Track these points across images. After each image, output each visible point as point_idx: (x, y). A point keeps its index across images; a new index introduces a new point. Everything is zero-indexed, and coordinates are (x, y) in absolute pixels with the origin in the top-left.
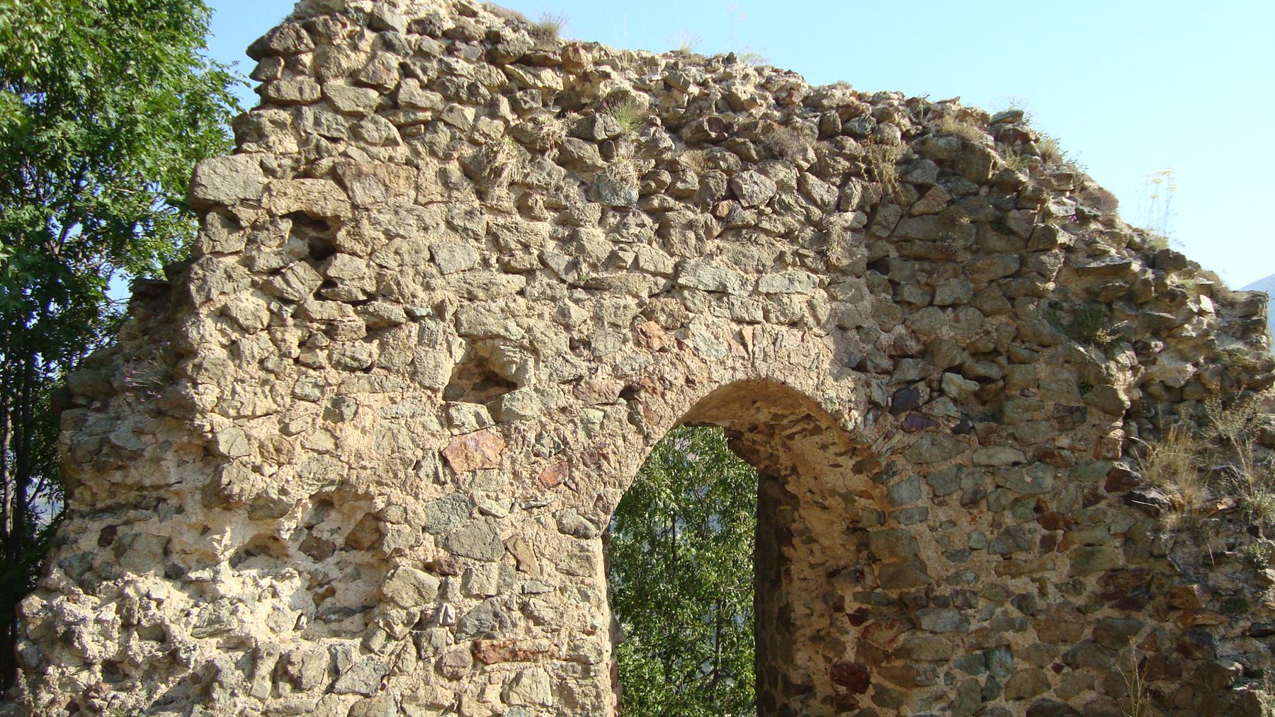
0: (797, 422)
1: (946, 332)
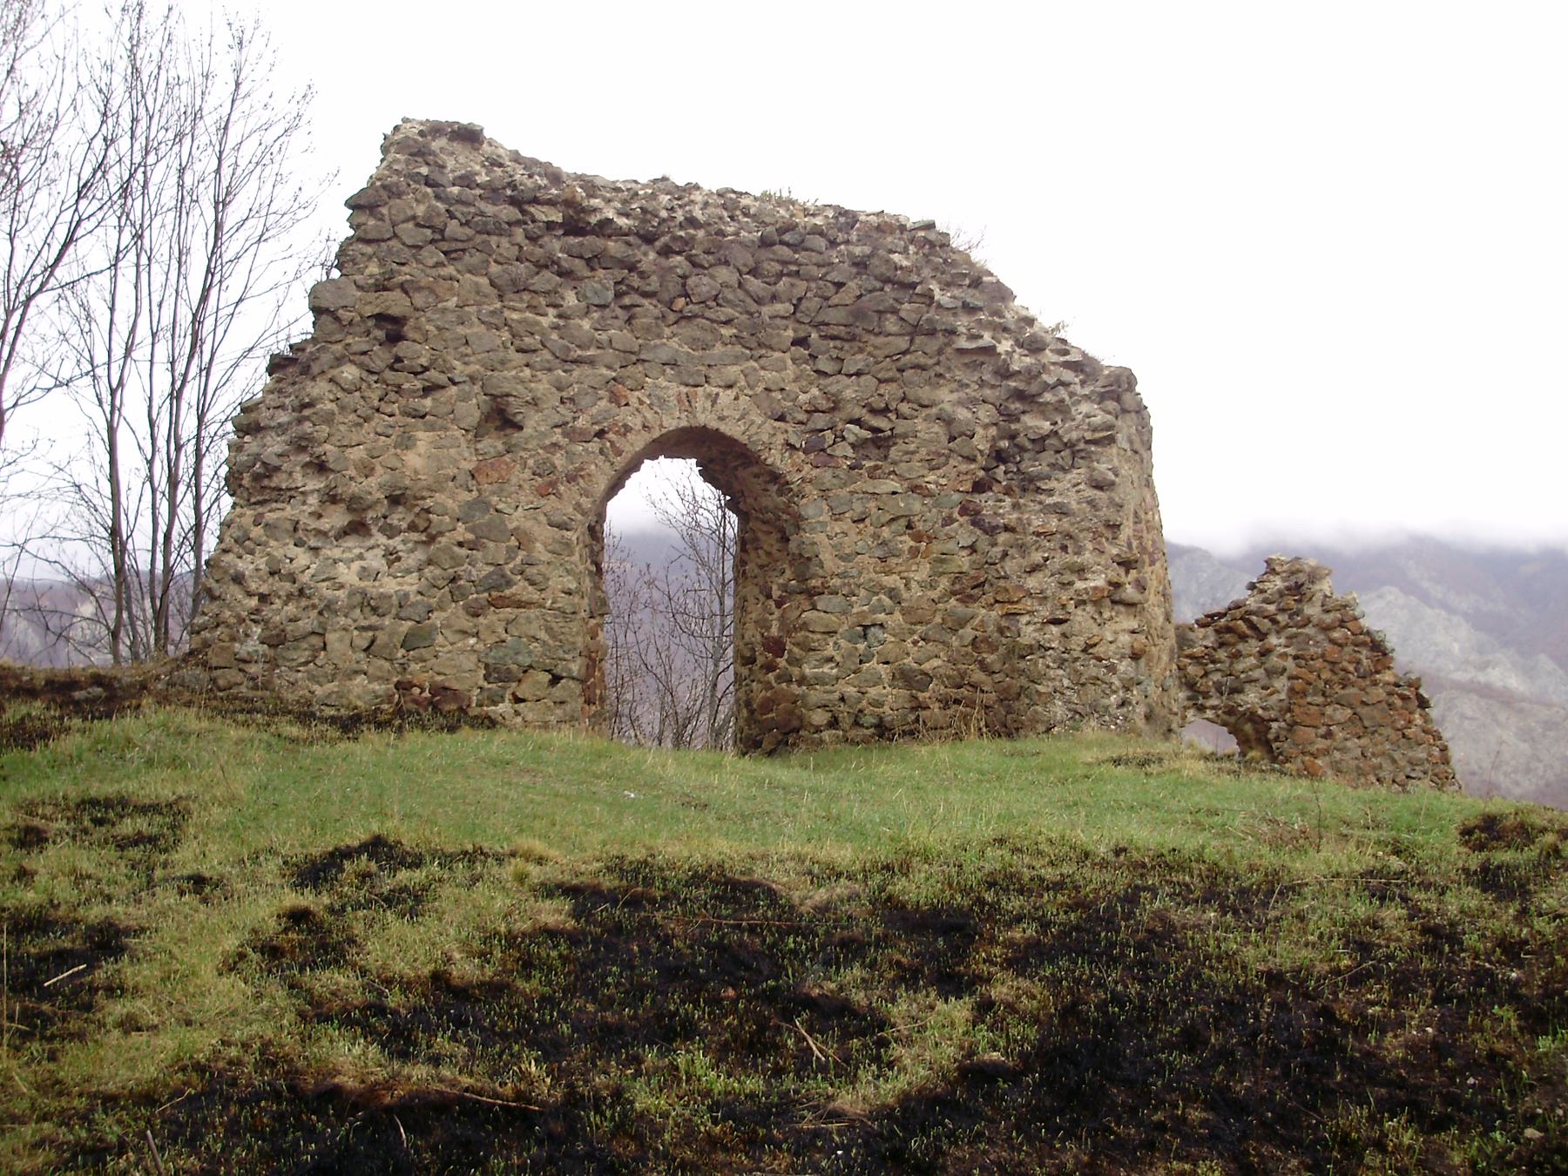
1: (849, 394)
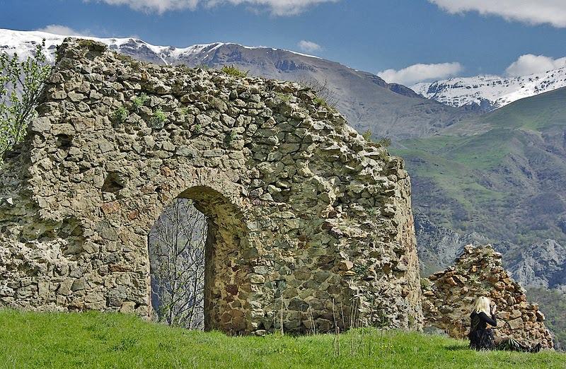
0: (216, 200)
